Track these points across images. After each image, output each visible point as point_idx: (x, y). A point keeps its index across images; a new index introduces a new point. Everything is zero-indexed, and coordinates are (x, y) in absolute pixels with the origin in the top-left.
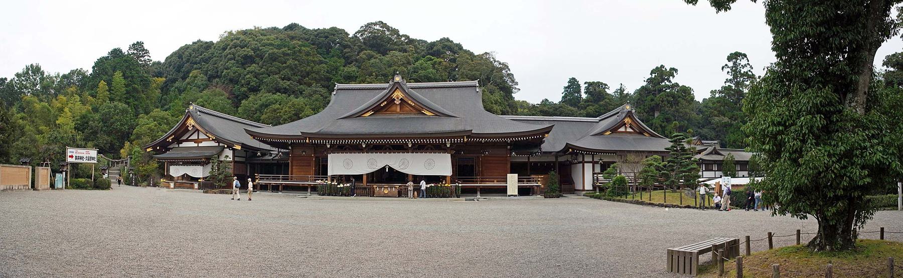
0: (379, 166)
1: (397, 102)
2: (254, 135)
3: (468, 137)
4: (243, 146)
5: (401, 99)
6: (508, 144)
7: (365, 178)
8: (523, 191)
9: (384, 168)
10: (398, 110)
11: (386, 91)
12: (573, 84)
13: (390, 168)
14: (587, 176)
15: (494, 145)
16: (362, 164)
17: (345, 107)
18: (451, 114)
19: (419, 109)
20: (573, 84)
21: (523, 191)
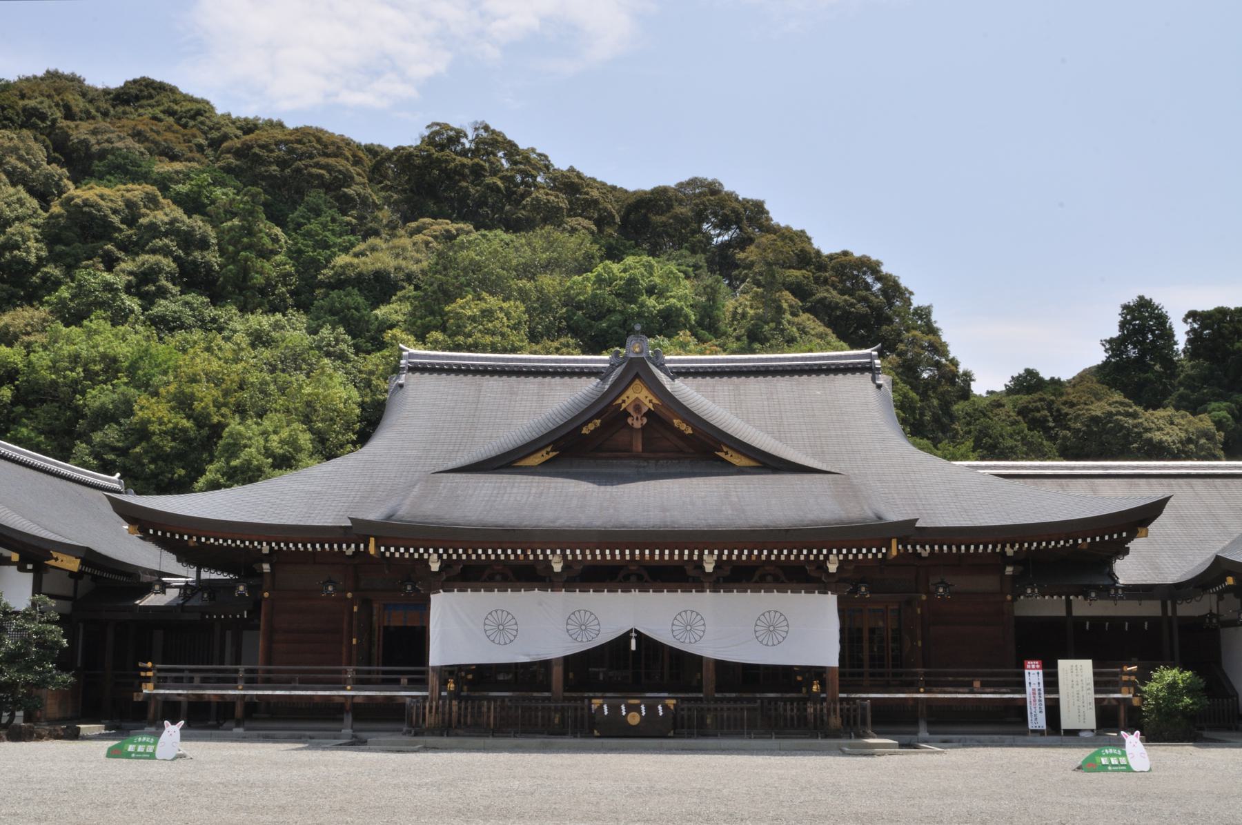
0: (607, 632)
1: (637, 423)
2: (143, 523)
3: (903, 541)
4: (90, 557)
5: (649, 414)
6: (1004, 559)
7: (557, 673)
8: (1112, 720)
9: (625, 637)
10: (638, 446)
11: (587, 388)
12: (1142, 321)
13: (641, 637)
14: (498, 577)
15: (959, 564)
16: (546, 627)
17: (441, 436)
18: (824, 468)
19: (706, 450)
20: (1142, 321)
21: (1112, 720)
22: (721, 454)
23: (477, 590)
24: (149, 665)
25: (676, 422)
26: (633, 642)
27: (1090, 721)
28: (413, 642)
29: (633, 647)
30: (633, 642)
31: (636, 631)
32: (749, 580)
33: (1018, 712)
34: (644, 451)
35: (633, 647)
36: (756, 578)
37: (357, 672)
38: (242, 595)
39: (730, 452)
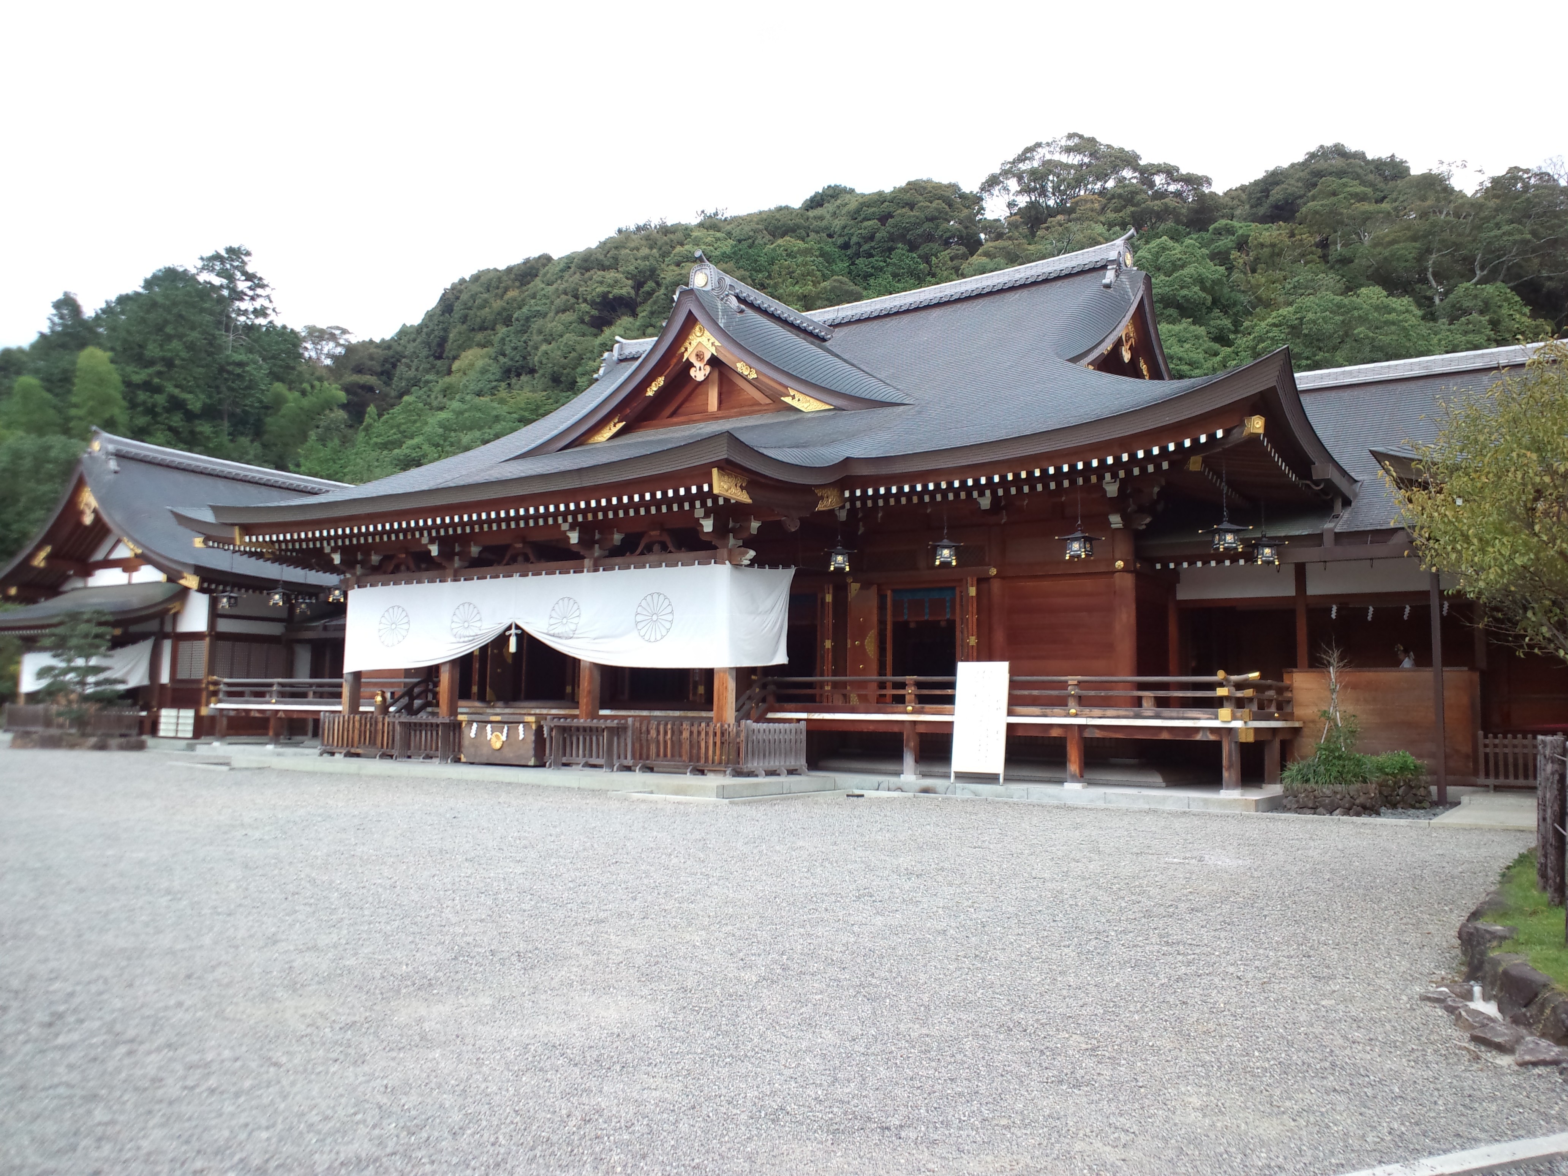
8: (1031, 753)
9: (502, 639)
13: (524, 638)
21: (1031, 753)
22: (787, 400)
23: (538, 574)
24: (1221, 675)
25: (650, 393)
26: (513, 642)
27: (996, 763)
28: (331, 651)
29: (1333, 616)
30: (513, 642)
31: (518, 627)
32: (499, 563)
33: (935, 748)
34: (719, 408)
35: (1333, 616)
36: (507, 558)
37: (919, 685)
38: (945, 565)
39: (798, 395)
